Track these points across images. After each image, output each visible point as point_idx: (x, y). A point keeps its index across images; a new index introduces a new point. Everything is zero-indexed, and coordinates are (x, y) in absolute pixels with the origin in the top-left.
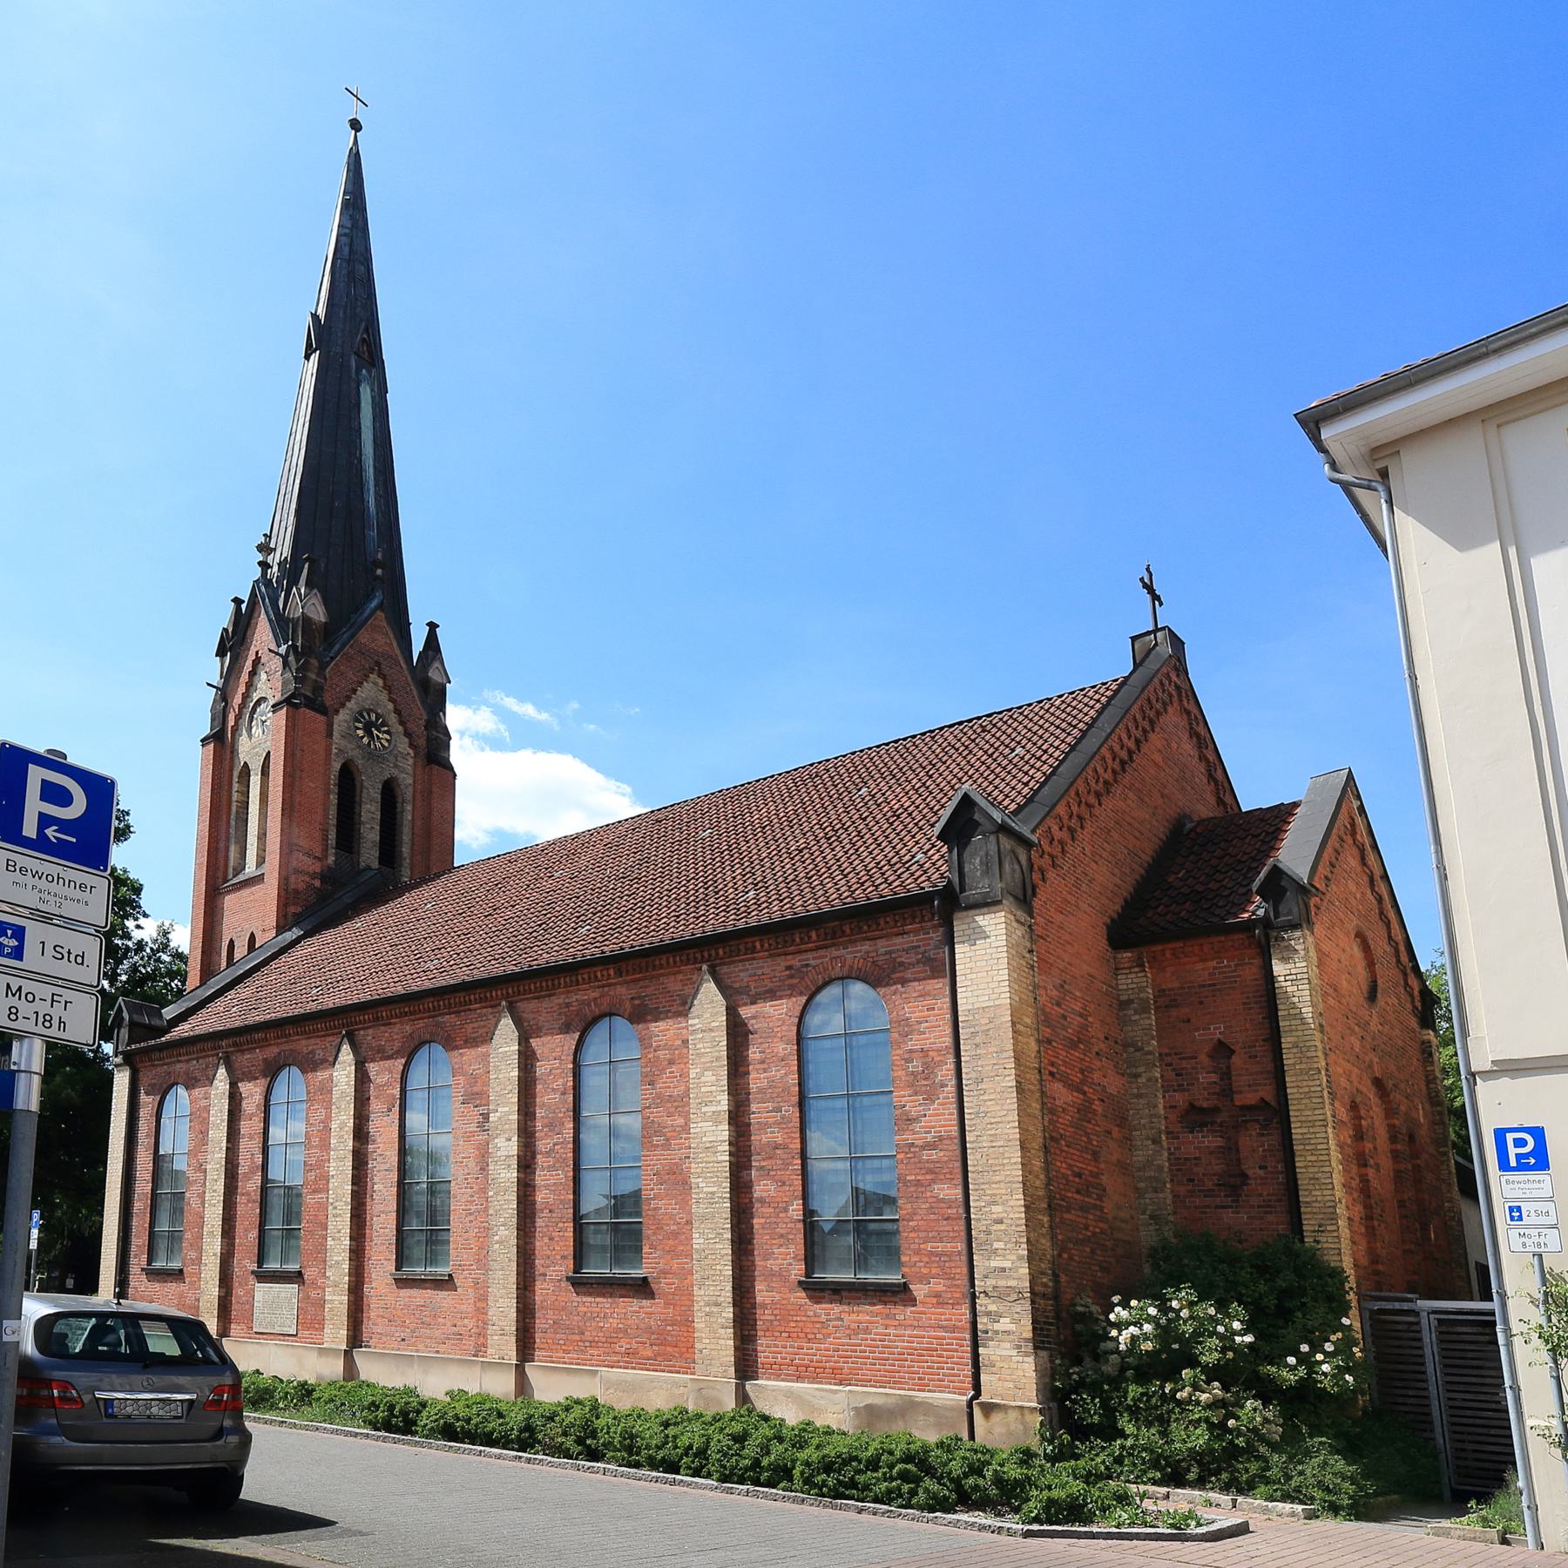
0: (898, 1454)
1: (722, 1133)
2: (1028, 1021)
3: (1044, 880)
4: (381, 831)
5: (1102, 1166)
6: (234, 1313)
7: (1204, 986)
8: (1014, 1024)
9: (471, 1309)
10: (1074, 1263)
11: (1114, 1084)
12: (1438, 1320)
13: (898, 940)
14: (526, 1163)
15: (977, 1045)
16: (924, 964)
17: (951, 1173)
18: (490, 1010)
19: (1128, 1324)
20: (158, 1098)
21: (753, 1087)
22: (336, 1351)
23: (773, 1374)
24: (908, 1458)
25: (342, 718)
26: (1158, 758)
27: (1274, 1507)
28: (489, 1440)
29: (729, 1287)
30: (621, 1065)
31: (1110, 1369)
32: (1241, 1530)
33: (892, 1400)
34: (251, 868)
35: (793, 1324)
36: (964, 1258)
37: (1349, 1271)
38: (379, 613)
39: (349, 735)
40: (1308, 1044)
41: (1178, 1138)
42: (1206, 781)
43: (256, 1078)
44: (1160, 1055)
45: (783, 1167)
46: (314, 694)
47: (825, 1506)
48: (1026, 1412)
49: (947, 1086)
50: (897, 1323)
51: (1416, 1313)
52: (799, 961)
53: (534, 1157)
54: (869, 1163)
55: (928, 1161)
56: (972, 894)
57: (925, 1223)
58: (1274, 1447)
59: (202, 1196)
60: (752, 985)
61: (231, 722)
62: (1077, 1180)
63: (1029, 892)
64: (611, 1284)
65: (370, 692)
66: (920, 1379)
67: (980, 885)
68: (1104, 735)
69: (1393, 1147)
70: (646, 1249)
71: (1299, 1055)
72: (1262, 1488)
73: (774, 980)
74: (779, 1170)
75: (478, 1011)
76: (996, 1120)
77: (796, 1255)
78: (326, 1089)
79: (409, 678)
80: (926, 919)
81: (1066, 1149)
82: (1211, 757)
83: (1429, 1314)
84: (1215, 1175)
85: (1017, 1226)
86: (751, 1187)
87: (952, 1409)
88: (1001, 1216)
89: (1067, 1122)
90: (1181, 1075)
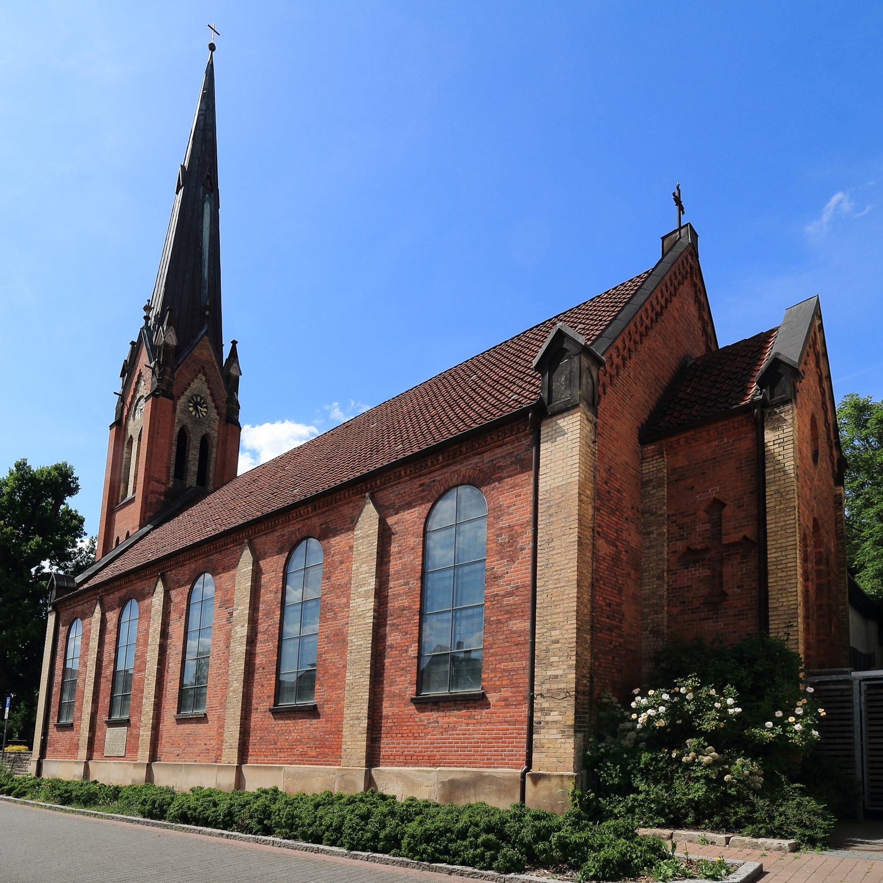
0: (482, 825)
1: (369, 604)
3: (605, 393)
4: (199, 465)
5: (623, 598)
6: (95, 746)
7: (707, 461)
8: (580, 494)
9: (215, 733)
10: (601, 668)
11: (632, 538)
12: (868, 685)
13: (498, 451)
14: (251, 641)
15: (551, 515)
17: (522, 612)
18: (238, 547)
19: (646, 709)
20: (68, 627)
21: (392, 571)
22: (143, 764)
23: (389, 762)
24: (489, 829)
25: (182, 400)
26: (676, 315)
27: (763, 844)
28: (207, 824)
29: (366, 706)
30: (311, 570)
31: (628, 743)
33: (466, 776)
34: (130, 495)
35: (405, 728)
36: (527, 671)
37: (802, 656)
39: (185, 411)
40: (787, 489)
41: (676, 574)
42: (701, 333)
43: (114, 609)
44: (668, 516)
45: (407, 622)
47: (424, 869)
48: (565, 779)
49: (525, 549)
50: (475, 721)
51: (849, 682)
53: (256, 636)
54: (464, 613)
55: (507, 605)
56: (557, 404)
58: (759, 793)
59: (84, 681)
60: (397, 501)
61: (125, 414)
63: (597, 398)
64: (295, 711)
65: (198, 385)
66: (488, 759)
67: (563, 394)
68: (648, 292)
69: (818, 568)
70: (317, 687)
71: (780, 498)
72: (750, 828)
74: (405, 624)
76: (561, 568)
77: (411, 681)
78: (148, 610)
79: (220, 375)
80: (521, 430)
81: (603, 586)
82: (706, 317)
83: (860, 681)
84: (702, 597)
86: (385, 639)
87: (510, 779)
88: (557, 637)
90: (683, 528)
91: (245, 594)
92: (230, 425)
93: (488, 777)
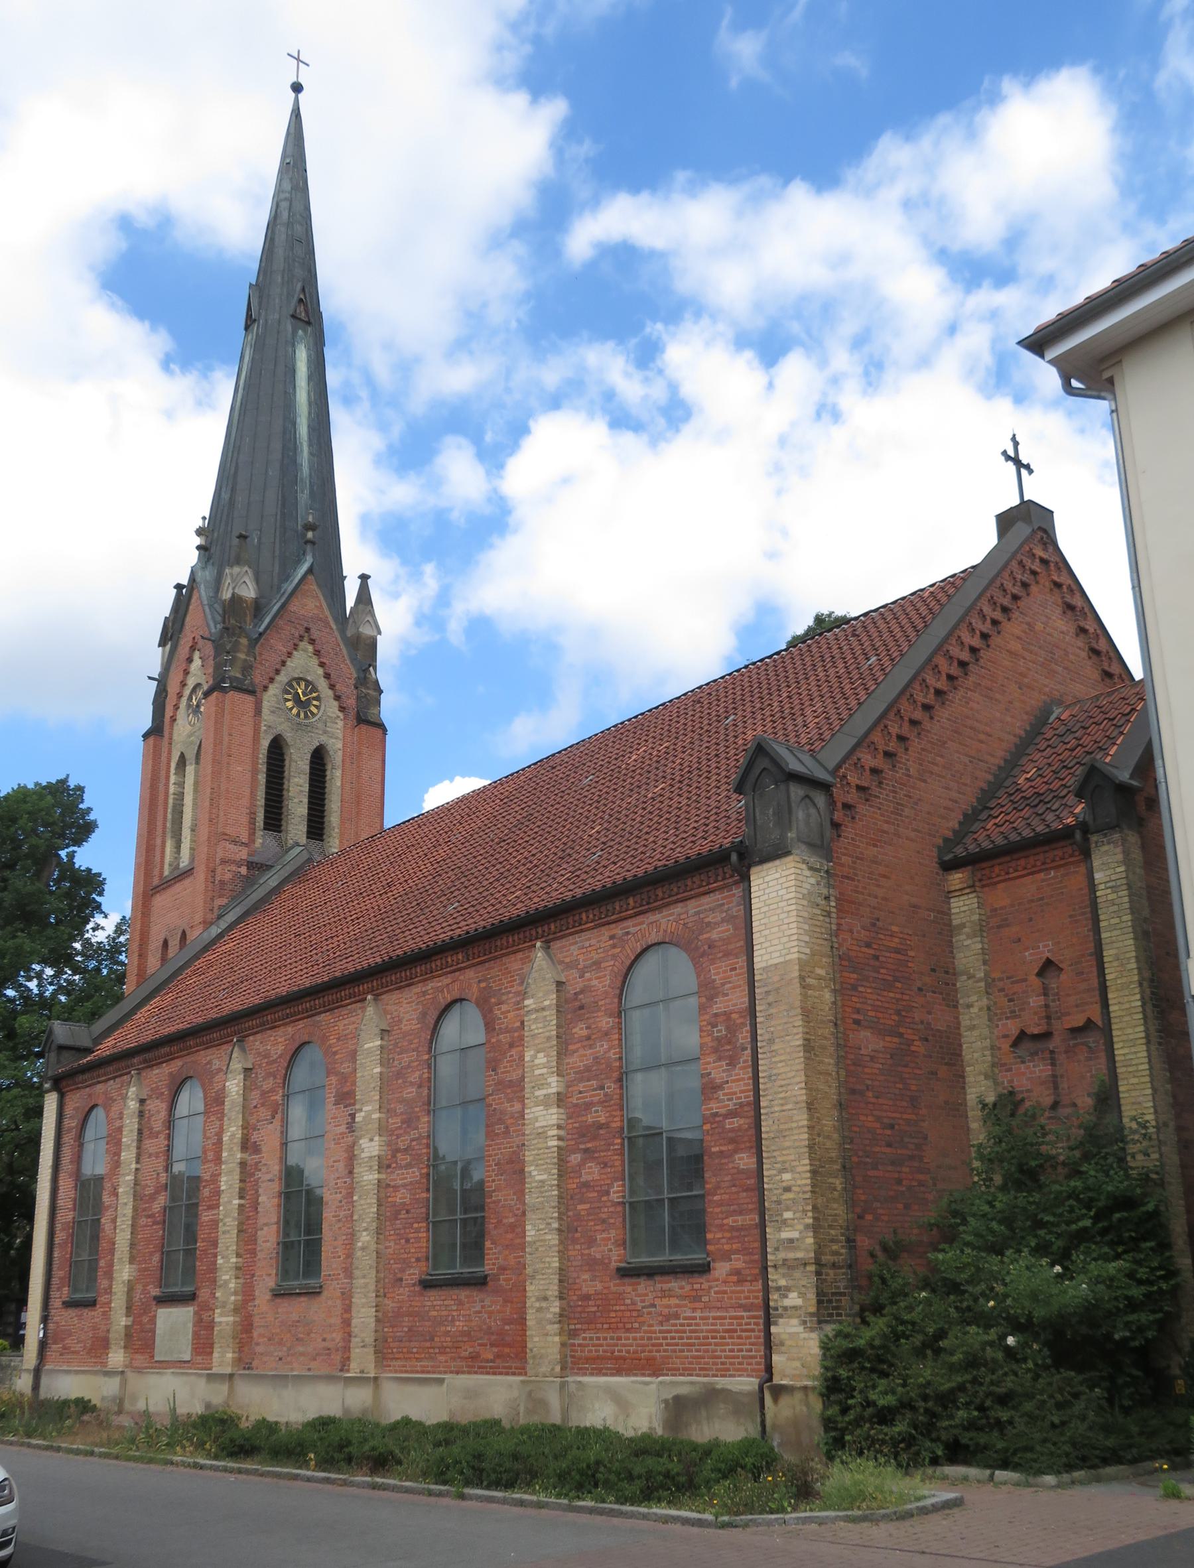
2: (821, 972)
7: (1032, 901)
15: (770, 1004)
16: (728, 921)
18: (359, 1005)
32: (957, 1503)
35: (613, 1315)
38: (310, 577)
41: (1010, 1070)
46: (243, 675)
52: (621, 929)
55: (732, 1130)
57: (727, 1196)
59: (114, 1221)
60: (581, 958)
62: (888, 1132)
65: (303, 662)
66: (722, 1363)
73: (599, 951)
75: (349, 1007)
80: (727, 876)
81: (873, 1100)
85: (804, 1192)
89: (877, 1072)
91: (372, 1085)
92: (364, 727)
93: (723, 1390)
